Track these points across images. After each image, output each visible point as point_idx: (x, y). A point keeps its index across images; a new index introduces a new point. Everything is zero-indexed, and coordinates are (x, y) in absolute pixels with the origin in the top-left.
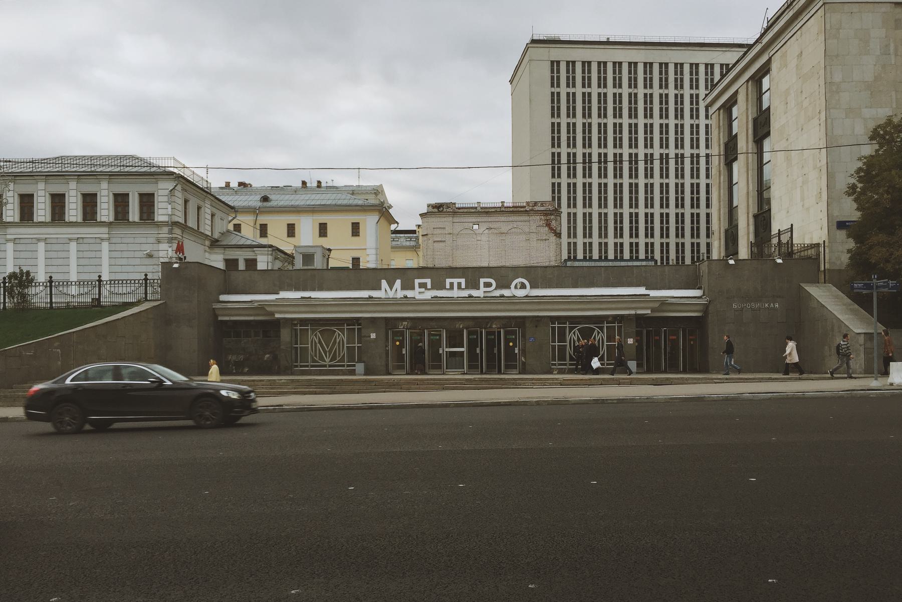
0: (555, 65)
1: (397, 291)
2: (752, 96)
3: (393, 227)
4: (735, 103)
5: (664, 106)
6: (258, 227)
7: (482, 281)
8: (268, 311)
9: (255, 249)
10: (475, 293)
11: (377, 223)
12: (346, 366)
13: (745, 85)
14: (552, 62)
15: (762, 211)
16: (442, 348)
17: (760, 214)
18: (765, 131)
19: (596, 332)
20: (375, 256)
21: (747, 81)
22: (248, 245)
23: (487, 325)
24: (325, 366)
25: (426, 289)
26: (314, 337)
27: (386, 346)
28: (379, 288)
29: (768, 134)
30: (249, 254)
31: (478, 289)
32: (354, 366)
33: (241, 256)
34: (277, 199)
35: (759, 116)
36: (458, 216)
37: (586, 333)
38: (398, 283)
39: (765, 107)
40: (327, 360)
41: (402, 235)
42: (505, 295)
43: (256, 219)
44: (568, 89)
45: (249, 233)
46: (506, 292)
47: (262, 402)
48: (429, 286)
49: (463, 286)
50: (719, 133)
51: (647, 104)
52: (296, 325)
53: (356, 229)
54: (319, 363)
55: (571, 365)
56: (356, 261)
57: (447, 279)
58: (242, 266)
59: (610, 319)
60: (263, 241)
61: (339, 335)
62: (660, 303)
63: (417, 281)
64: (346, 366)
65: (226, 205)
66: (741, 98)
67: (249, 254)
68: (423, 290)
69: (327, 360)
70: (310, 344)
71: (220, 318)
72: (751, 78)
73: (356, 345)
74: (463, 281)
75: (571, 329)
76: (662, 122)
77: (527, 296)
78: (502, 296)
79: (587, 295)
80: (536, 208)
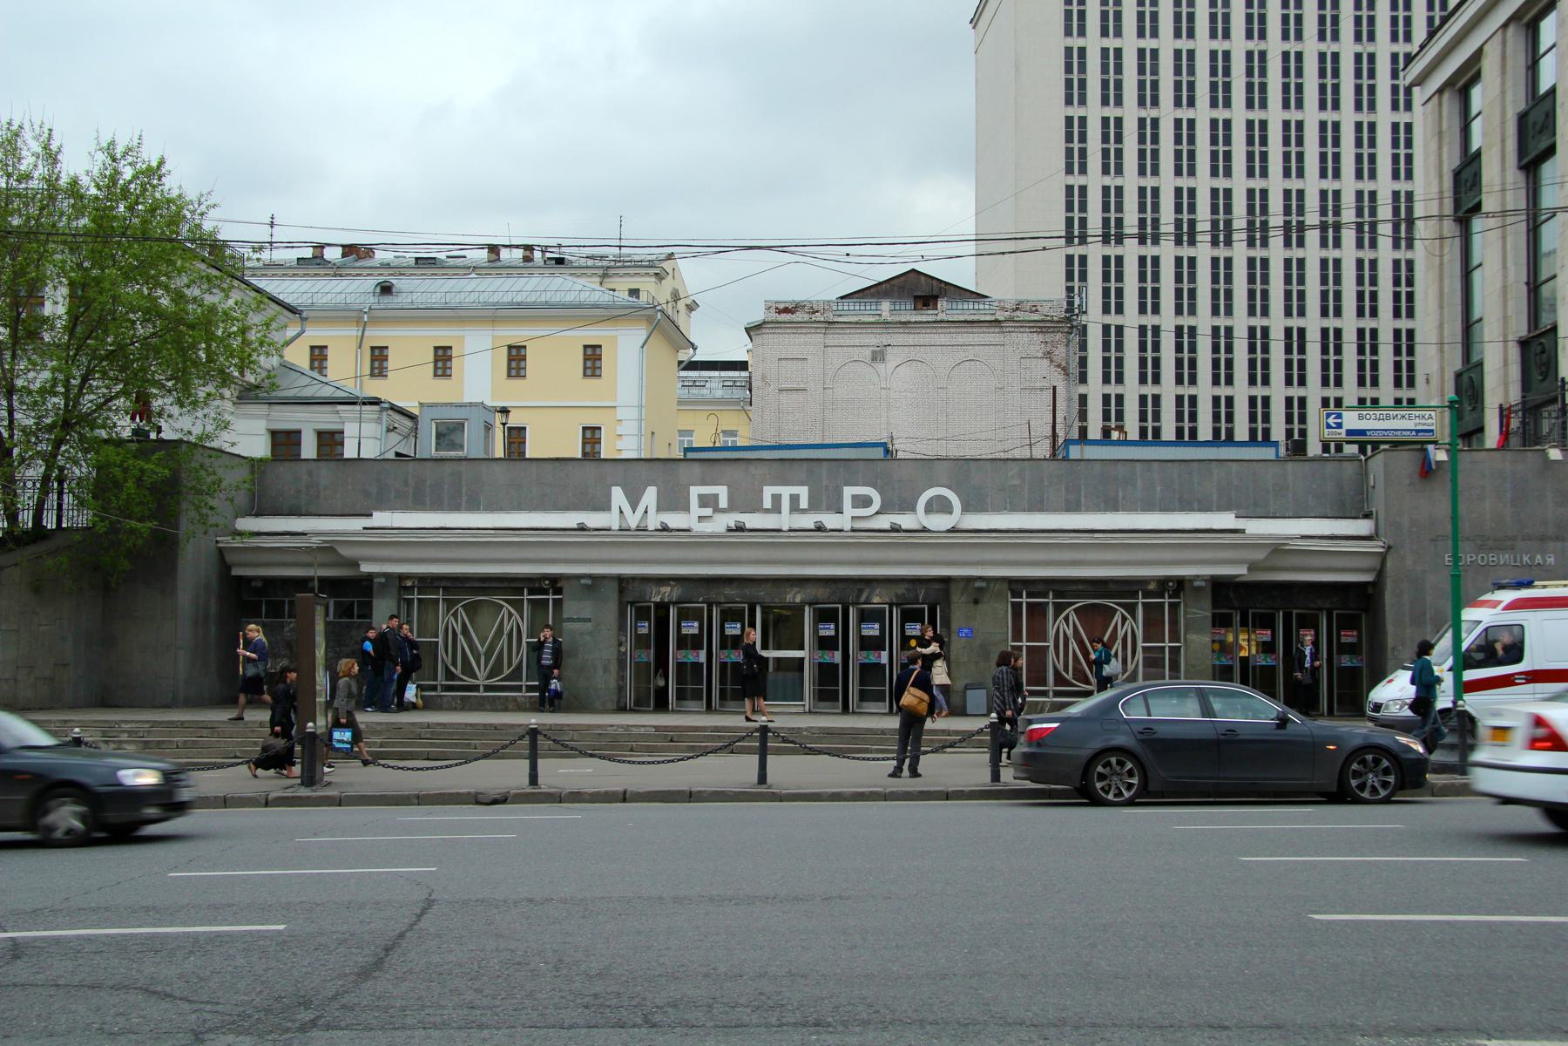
1: (648, 511)
2: (1519, 61)
3: (686, 355)
4: (1476, 78)
5: (1329, 81)
6: (368, 353)
7: (849, 492)
8: (342, 556)
9: (340, 407)
10: (830, 520)
11: (642, 347)
12: (524, 688)
13: (1499, 36)
15: (1538, 332)
16: (705, 651)
17: (1532, 337)
18: (1544, 145)
19: (1117, 618)
20: (636, 424)
21: (1505, 26)
22: (325, 398)
23: (859, 596)
25: (717, 510)
26: (452, 619)
27: (620, 644)
28: (605, 506)
29: (1551, 151)
30: (325, 419)
31: (686, 509)
33: (308, 423)
34: (411, 290)
35: (1531, 109)
36: (838, 331)
37: (1096, 618)
38: (650, 496)
39: (1544, 87)
40: (481, 674)
41: (716, 373)
42: (748, 526)
43: (363, 335)
44: (1104, 39)
45: (345, 370)
46: (906, 521)
48: (723, 503)
49: (804, 504)
50: (1440, 148)
51: (1079, 79)
52: (410, 590)
53: (592, 359)
54: (462, 680)
55: (530, 689)
56: (591, 435)
57: (725, 488)
58: (309, 449)
59: (1152, 587)
60: (374, 388)
61: (510, 615)
62: (1269, 550)
63: (695, 491)
64: (524, 688)
65: (279, 304)
66: (1489, 66)
67: (325, 419)
68: (708, 511)
69: (481, 674)
70: (441, 636)
71: (236, 572)
72: (1515, 18)
74: (803, 492)
75: (1059, 609)
76: (1070, 114)
77: (953, 530)
78: (895, 529)
79: (1215, 527)
80: (1020, 315)
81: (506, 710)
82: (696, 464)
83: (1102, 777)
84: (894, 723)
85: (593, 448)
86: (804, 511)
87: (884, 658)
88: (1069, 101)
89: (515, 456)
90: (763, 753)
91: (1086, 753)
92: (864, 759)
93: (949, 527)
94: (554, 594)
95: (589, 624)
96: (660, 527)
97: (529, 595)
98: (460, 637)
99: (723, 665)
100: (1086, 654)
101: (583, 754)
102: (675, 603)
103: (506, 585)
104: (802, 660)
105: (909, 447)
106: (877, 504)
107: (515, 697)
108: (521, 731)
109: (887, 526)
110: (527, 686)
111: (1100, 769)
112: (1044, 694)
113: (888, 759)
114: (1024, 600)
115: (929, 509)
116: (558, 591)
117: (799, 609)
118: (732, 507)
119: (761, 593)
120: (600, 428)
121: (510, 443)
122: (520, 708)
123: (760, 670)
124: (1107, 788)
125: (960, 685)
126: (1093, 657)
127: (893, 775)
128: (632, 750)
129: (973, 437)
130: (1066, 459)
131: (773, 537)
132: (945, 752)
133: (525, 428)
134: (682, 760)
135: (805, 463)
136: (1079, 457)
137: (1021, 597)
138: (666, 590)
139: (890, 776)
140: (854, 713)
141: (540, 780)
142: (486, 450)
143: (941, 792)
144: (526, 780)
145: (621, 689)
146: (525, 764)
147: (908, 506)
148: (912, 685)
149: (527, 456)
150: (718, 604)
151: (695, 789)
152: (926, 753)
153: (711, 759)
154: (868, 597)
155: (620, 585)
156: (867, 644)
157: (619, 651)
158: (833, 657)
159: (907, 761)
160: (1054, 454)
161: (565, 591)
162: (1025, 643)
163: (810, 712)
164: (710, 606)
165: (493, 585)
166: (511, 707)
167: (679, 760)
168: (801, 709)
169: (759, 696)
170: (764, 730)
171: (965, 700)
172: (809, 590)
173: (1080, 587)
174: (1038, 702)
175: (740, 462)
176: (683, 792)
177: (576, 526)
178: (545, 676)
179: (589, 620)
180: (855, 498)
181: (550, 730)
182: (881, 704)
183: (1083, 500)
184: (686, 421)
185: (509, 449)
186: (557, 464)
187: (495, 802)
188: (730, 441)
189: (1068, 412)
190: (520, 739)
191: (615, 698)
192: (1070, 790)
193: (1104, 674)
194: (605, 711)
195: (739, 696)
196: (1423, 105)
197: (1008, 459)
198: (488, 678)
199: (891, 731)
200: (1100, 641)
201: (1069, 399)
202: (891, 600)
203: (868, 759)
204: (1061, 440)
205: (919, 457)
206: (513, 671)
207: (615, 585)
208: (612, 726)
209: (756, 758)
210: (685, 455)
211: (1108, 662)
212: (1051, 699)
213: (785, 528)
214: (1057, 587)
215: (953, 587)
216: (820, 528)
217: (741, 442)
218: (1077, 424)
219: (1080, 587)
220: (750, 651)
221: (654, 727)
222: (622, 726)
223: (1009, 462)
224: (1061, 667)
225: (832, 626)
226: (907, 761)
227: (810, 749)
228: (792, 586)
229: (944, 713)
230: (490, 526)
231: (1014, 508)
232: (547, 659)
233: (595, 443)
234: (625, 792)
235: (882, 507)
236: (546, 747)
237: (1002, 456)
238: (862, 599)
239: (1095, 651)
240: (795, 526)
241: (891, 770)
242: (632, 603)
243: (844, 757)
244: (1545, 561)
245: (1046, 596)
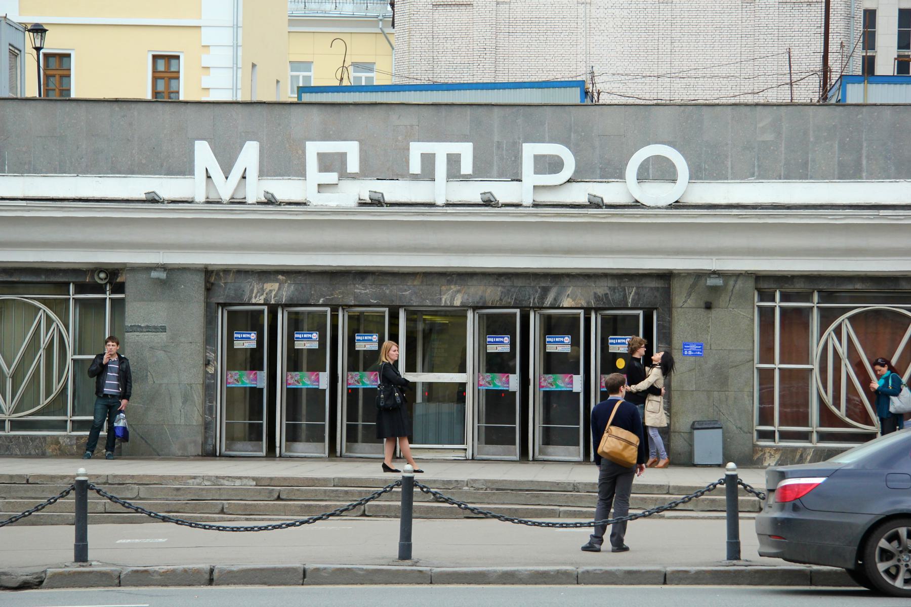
7: (530, 151)
10: (504, 191)
12: (69, 425)
20: (229, 52)
25: (344, 175)
27: (207, 363)
28: (185, 169)
31: (301, 172)
42: (388, 198)
48: (353, 166)
49: (467, 167)
55: (78, 426)
61: (49, 321)
63: (313, 149)
64: (69, 425)
68: (332, 177)
74: (465, 150)
75: (827, 317)
77: (677, 205)
78: (595, 204)
81: (43, 455)
82: (315, 110)
83: (886, 555)
84: (592, 475)
85: (168, 86)
86: (466, 178)
87: (577, 383)
89: (53, 95)
90: (407, 516)
91: (863, 521)
92: (548, 525)
93: (671, 201)
94: (113, 292)
95: (163, 335)
96: (263, 199)
97: (76, 292)
99: (353, 394)
100: (866, 382)
101: (154, 517)
102: (284, 306)
103: (43, 278)
104: (463, 385)
105: (616, 87)
106: (569, 170)
107: (57, 437)
108: (64, 485)
109: (584, 200)
110: (73, 422)
111: (883, 543)
112: (805, 436)
113: (582, 525)
114: (778, 304)
115: (643, 176)
116: (119, 288)
117: (459, 315)
118: (365, 172)
119: (408, 293)
120: (178, 57)
121: (47, 77)
122: (63, 453)
123: (404, 399)
124: (893, 571)
125: (683, 423)
126: (876, 385)
127: (589, 548)
128: (222, 512)
129: (708, 72)
130: (841, 104)
131: (423, 214)
132: (663, 517)
133: (69, 56)
134: (293, 525)
135: (468, 110)
136: (861, 101)
137: (773, 300)
138: (272, 287)
139: (585, 549)
140: (534, 460)
141: (91, 555)
142: (13, 87)
143: (658, 572)
144: (71, 555)
145: (207, 426)
146: (69, 533)
147: (615, 172)
148: (612, 424)
149: (73, 95)
150: (346, 307)
151: (310, 566)
152: (636, 517)
153: (333, 523)
154: (555, 299)
155: (207, 281)
156: (553, 364)
157: (207, 372)
158: (508, 382)
159: (609, 529)
160: (824, 97)
161: (129, 288)
162: (777, 365)
163: (473, 459)
164: (335, 309)
165: (23, 279)
166: (49, 451)
167: (288, 525)
168: (461, 455)
169: (402, 436)
170: (409, 484)
171: (691, 445)
172: (472, 290)
173: (859, 286)
174: (796, 449)
175: (378, 107)
176: (294, 570)
177: (143, 197)
178: (111, 408)
179: (163, 329)
180: (538, 159)
181: (105, 483)
182: (572, 448)
183: (864, 162)
184: (301, 49)
185: (47, 84)
186: (116, 107)
187: (25, 586)
188: (363, 78)
189: (848, 36)
190: (62, 497)
191: (200, 439)
192: (841, 573)
193: (892, 409)
194: (185, 457)
195: (377, 435)
197: (757, 105)
198: (16, 411)
199: (588, 487)
200: (886, 362)
201: (849, 17)
202: (588, 303)
203: (554, 525)
204: (834, 77)
205: (631, 101)
206: (54, 401)
207: (200, 280)
208: (195, 478)
209: (395, 525)
210: (299, 97)
211: (897, 392)
212: (814, 444)
213: (440, 201)
214: (824, 286)
215: (676, 284)
216: (488, 202)
217: (379, 79)
218: (860, 53)
219: (859, 286)
220: (389, 374)
221: (254, 479)
222: (209, 478)
223: (759, 108)
224: (829, 400)
225: (507, 339)
226: (609, 529)
227: (472, 510)
228: (449, 282)
229: (662, 463)
230: (20, 195)
231: (763, 174)
232: (111, 386)
233: (170, 78)
234: (212, 571)
235: (576, 172)
236: (100, 508)
237: (750, 99)
238: (548, 301)
239: (879, 377)
240: (455, 199)
241: (586, 541)
242: (224, 305)
243: (520, 522)
245: (807, 297)
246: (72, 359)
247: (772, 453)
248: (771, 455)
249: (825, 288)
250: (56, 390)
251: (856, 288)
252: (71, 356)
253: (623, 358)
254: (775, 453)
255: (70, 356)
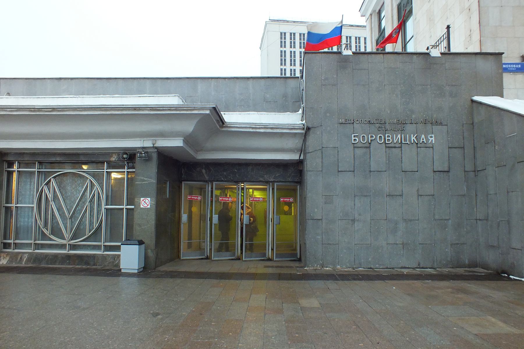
0: (283, 35)
14: (281, 33)
24: (63, 246)
32: (118, 248)
47: (229, 117)
54: (51, 240)
59: (113, 159)
73: (124, 207)
88: (281, 64)
98: (52, 204)
196: (366, 22)
214: (40, 159)
244: (427, 140)
246: (105, 208)
247: (5, 257)
248: (4, 257)
249: (40, 160)
250: (96, 226)
251: (57, 160)
252: (104, 205)
253: (288, 206)
254: (6, 257)
255: (103, 207)
